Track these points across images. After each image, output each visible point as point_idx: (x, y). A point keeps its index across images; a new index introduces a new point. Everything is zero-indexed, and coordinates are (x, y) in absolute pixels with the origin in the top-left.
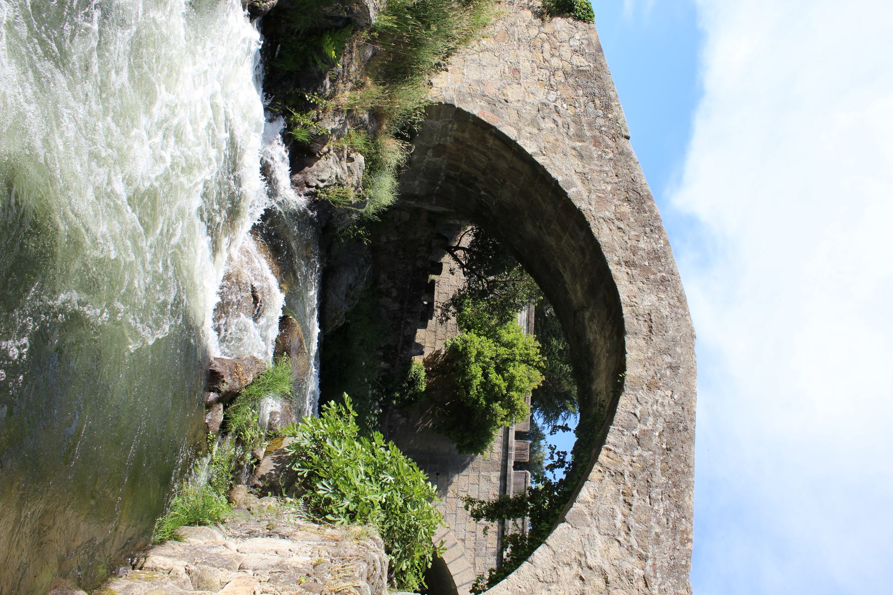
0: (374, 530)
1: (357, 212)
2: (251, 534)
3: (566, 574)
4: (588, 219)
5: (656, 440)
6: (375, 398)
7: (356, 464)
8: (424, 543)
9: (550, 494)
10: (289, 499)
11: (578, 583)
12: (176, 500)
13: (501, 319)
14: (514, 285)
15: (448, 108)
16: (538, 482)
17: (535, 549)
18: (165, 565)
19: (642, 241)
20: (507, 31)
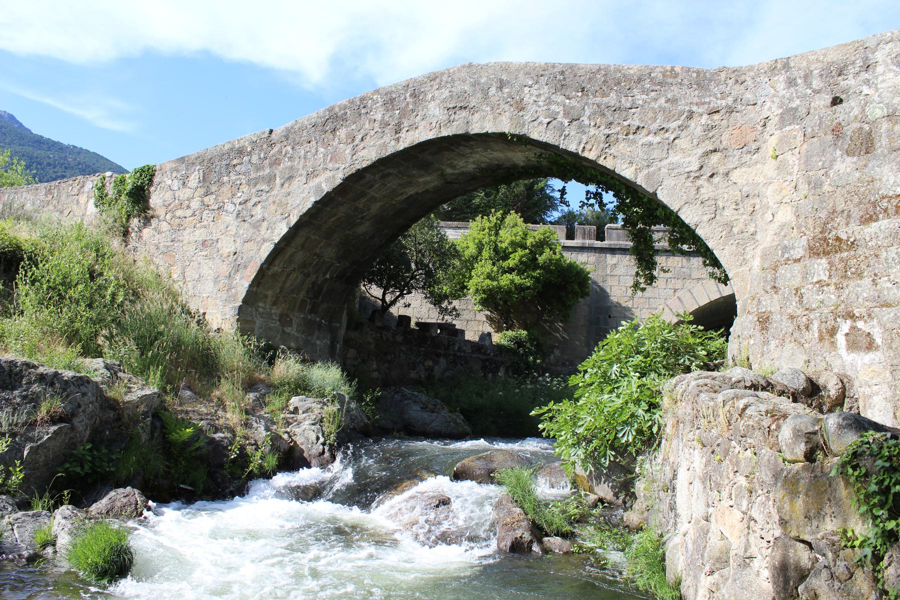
0: (667, 384)
1: (349, 403)
2: (672, 508)
3: (707, 191)
4: (354, 171)
5: (573, 103)
6: (534, 381)
7: (601, 403)
8: (679, 333)
9: (628, 207)
10: (637, 470)
11: (716, 179)
12: (640, 583)
13: (454, 256)
14: (420, 244)
16: (616, 219)
17: (683, 223)
18: (705, 596)
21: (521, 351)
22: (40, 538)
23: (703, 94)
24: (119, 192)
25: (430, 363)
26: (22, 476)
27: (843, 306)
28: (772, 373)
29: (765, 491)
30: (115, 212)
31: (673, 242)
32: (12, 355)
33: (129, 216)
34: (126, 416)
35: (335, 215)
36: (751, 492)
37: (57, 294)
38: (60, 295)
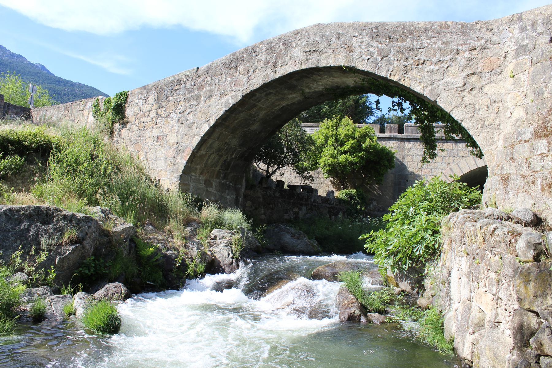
0: (444, 219)
1: (247, 233)
2: (448, 295)
3: (468, 99)
4: (248, 91)
5: (384, 46)
6: (361, 220)
8: (451, 188)
11: (474, 92)
14: (289, 136)
16: (411, 119)
19: (261, 58)
20: (134, 144)
21: (352, 202)
23: (465, 38)
24: (107, 108)
25: (297, 210)
26: (55, 275)
28: (511, 211)
29: (508, 281)
30: (105, 120)
31: (447, 133)
33: (113, 122)
34: (114, 240)
35: (238, 119)
36: (499, 282)
37: (72, 169)
38: (74, 169)
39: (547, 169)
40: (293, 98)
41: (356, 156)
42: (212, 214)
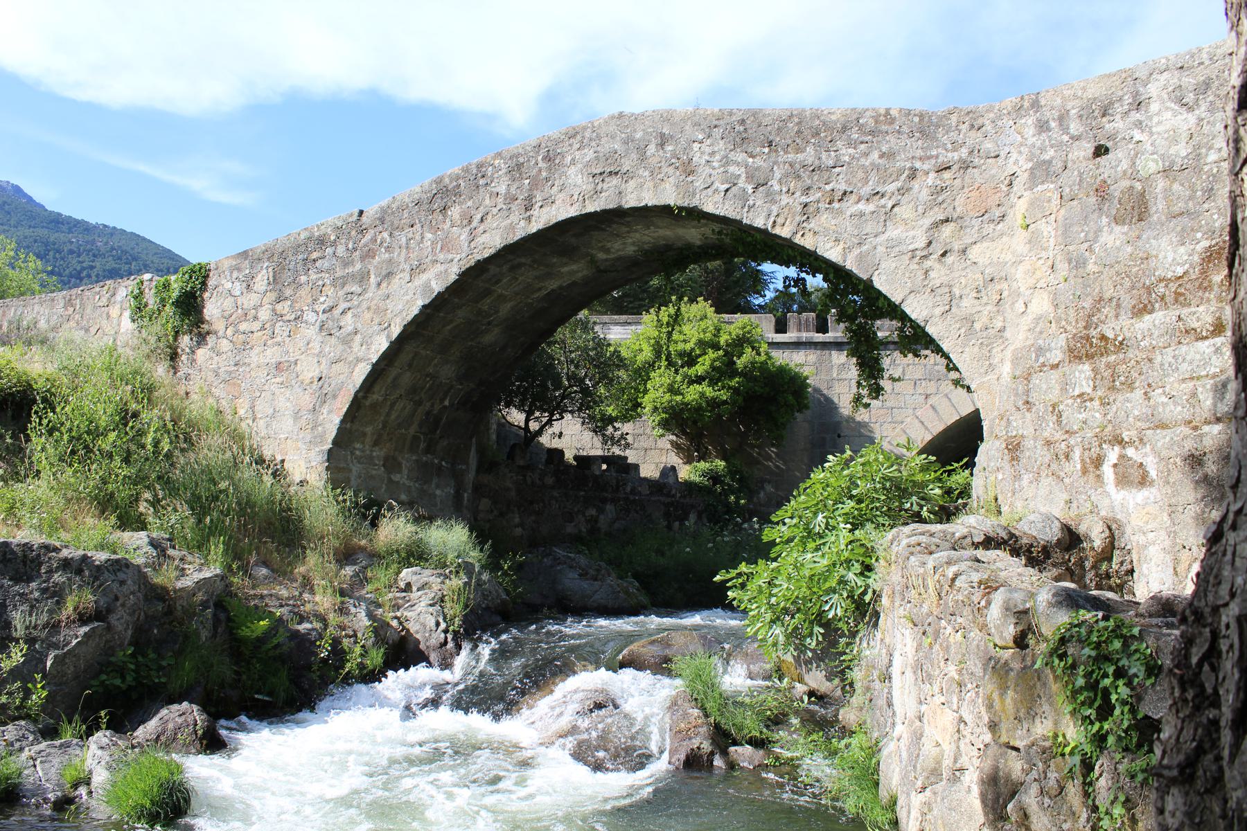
1: (480, 573)
2: (890, 705)
3: (938, 275)
4: (472, 263)
5: (759, 162)
11: (950, 259)
13: (618, 367)
14: (571, 352)
15: (334, 456)
20: (224, 381)
21: (718, 488)
22: (70, 775)
23: (921, 144)
24: (163, 300)
25: (593, 512)
26: (45, 694)
27: (1110, 428)
30: (157, 328)
32: (25, 535)
33: (177, 332)
34: (179, 608)
35: (451, 321)
39: (1091, 428)
40: (571, 273)
41: (723, 388)
42: (400, 534)
